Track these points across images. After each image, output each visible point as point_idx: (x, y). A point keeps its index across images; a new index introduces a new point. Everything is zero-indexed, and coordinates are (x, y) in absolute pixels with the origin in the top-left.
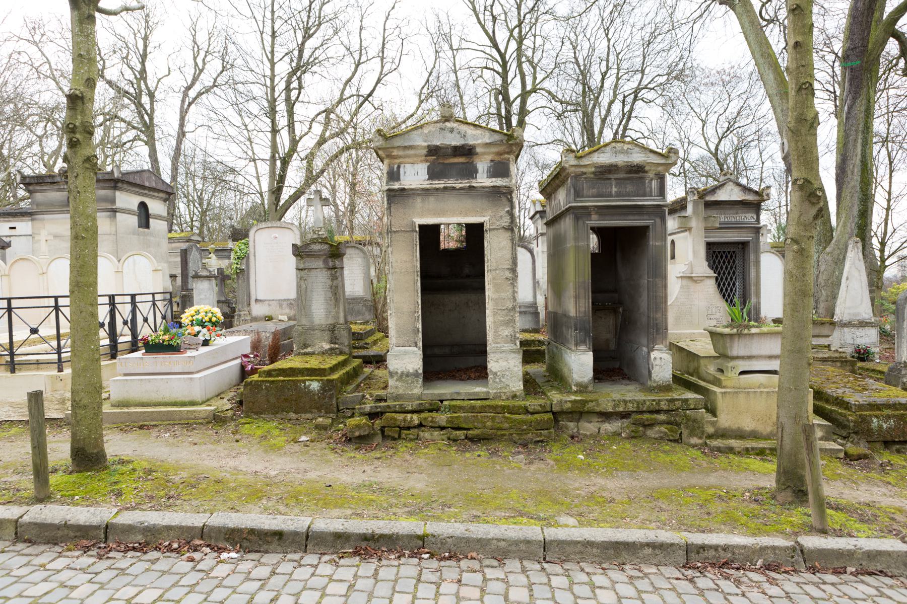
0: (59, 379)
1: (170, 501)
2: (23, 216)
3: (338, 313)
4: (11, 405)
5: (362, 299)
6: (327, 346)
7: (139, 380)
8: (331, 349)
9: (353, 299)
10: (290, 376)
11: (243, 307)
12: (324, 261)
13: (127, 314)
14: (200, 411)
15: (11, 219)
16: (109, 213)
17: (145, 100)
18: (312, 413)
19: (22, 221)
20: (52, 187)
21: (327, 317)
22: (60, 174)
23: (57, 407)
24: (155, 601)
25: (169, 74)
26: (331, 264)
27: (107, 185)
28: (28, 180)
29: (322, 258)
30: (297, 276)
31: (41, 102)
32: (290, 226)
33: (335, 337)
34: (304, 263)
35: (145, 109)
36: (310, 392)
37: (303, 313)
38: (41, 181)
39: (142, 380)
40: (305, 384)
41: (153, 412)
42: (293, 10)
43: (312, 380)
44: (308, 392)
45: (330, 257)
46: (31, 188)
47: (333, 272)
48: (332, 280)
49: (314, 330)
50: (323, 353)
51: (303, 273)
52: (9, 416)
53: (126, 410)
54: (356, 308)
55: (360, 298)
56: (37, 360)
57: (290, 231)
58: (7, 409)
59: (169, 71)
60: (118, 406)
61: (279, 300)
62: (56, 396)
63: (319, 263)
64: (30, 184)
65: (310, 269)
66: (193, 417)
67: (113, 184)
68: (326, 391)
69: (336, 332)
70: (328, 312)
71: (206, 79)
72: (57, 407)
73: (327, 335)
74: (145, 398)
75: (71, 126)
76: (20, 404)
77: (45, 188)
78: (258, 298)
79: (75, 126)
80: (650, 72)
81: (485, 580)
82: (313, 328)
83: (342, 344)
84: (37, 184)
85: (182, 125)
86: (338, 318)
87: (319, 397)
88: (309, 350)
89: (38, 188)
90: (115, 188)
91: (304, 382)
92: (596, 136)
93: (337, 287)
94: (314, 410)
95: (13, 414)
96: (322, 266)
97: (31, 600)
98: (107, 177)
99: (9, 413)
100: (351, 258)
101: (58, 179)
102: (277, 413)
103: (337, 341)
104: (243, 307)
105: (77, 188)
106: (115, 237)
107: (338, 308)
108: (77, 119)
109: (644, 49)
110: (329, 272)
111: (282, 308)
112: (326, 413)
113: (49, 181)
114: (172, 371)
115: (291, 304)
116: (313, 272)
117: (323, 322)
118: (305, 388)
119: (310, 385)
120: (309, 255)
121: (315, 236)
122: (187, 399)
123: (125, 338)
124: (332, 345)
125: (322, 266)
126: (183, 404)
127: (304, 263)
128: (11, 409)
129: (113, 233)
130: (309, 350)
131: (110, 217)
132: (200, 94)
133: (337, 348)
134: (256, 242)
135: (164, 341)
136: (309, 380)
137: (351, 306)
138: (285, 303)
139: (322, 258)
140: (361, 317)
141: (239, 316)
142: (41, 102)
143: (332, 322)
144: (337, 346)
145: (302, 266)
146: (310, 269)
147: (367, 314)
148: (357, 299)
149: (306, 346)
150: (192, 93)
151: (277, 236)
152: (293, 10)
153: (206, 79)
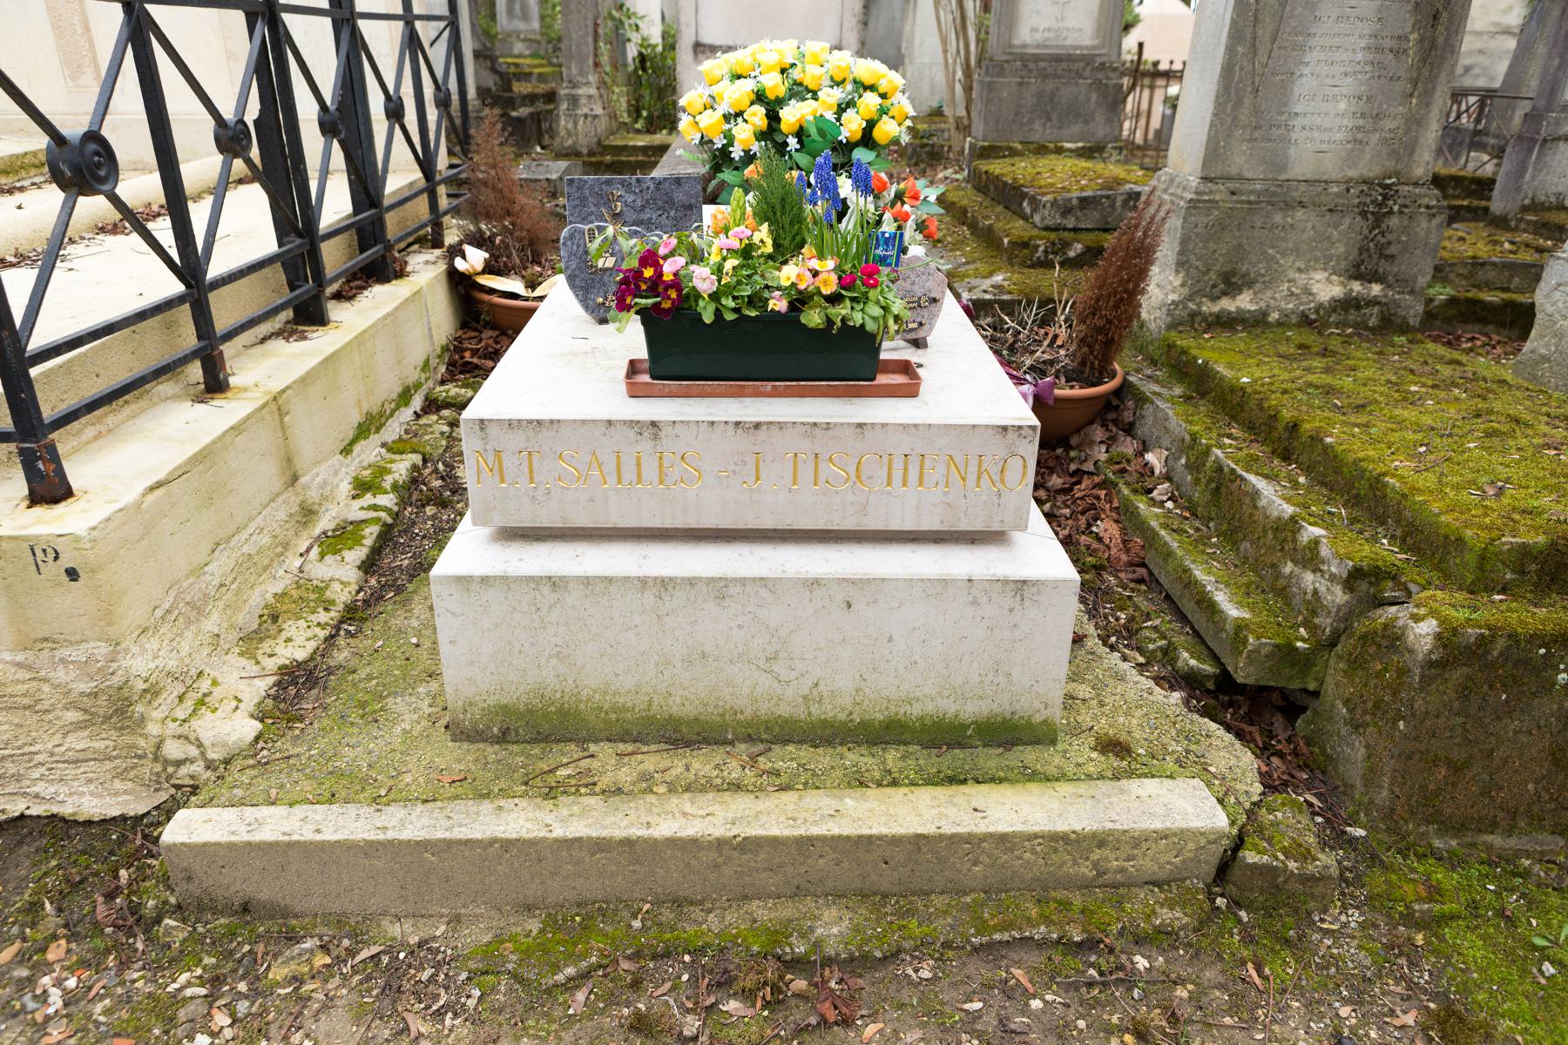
0: (54, 570)
3: (1415, 122)
5: (1088, 59)
6: (1326, 288)
8: (1348, 304)
9: (1057, 59)
11: (582, 73)
13: (326, 69)
21: (1357, 141)
31: (416, 597)
33: (1381, 248)
37: (1245, 110)
49: (1288, 206)
50: (1305, 321)
54: (1066, 93)
55: (1081, 58)
62: (60, 675)
69: (1394, 222)
70: (1370, 114)
73: (1345, 235)
78: (706, 39)
83: (1404, 283)
88: (1244, 302)
92: (255, 83)
103: (1384, 266)
104: (582, 73)
107: (1426, 103)
117: (1331, 167)
122: (972, 709)
123: (898, 465)
124: (1356, 287)
130: (1244, 302)
133: (1374, 302)
135: (800, 300)
137: (1050, 85)
140: (1075, 129)
141: (574, 101)
142: (416, 597)
143: (1374, 171)
144: (1376, 289)
148: (1069, 58)
149: (1231, 284)
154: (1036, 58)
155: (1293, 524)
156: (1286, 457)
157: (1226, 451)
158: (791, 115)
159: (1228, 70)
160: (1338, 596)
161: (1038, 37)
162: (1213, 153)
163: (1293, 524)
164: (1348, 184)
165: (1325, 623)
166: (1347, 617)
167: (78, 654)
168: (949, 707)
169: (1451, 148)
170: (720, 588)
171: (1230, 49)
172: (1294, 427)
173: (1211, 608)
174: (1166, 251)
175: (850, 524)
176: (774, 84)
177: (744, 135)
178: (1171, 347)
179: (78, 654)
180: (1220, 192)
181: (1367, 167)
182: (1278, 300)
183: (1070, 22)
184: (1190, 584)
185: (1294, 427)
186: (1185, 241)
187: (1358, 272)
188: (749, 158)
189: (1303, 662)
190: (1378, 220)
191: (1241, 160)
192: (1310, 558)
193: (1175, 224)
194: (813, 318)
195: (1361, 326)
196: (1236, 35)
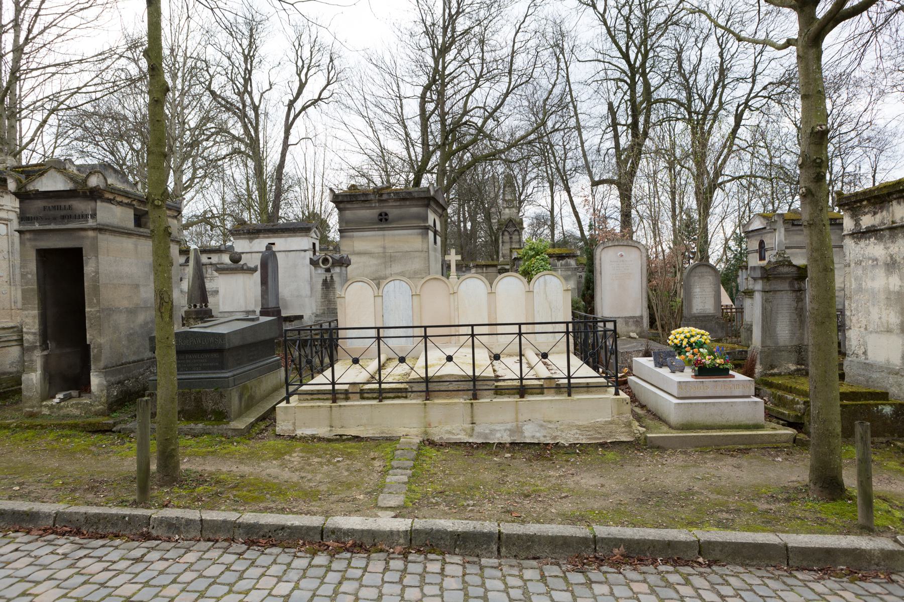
0: (625, 403)
1: (213, 502)
2: (284, 232)
4: (579, 427)
5: (713, 316)
6: (793, 367)
7: (703, 403)
8: (798, 370)
9: (705, 317)
10: (853, 400)
12: (790, 283)
14: (781, 435)
15: (270, 235)
16: (421, 231)
17: (251, 113)
18: (885, 436)
19: (281, 237)
20: (363, 205)
22: (374, 192)
23: (623, 430)
24: (55, 600)
25: (271, 88)
26: (796, 286)
27: (420, 203)
28: (340, 199)
29: (788, 281)
30: (762, 298)
32: (636, 245)
34: (770, 285)
35: (249, 119)
36: (883, 416)
38: (354, 199)
39: (706, 403)
40: (878, 408)
41: (735, 435)
42: (574, 29)
43: (884, 404)
44: (881, 416)
45: (796, 279)
46: (341, 206)
47: (799, 294)
48: (797, 302)
49: (781, 351)
50: (789, 374)
51: (768, 295)
52: (578, 439)
53: (709, 434)
56: (588, 383)
57: (635, 249)
58: (575, 431)
59: (271, 85)
60: (682, 429)
61: (625, 318)
63: (785, 286)
64: (341, 202)
65: (775, 291)
66: (774, 440)
67: (426, 202)
68: (898, 415)
69: (803, 353)
70: (793, 333)
71: (309, 94)
72: (623, 430)
73: (794, 356)
74: (709, 421)
75: (818, 161)
76: (588, 427)
77: (356, 206)
79: (822, 160)
80: (762, 81)
81: (384, 582)
82: (779, 349)
84: (348, 202)
85: (286, 137)
86: (803, 339)
87: (892, 421)
88: (776, 371)
89: (349, 206)
90: (428, 206)
91: (877, 405)
93: (802, 309)
94: (886, 434)
95: (581, 437)
96: (788, 289)
97: (124, 599)
98: (423, 195)
99: (577, 436)
100: (702, 276)
101: (372, 197)
102: (850, 437)
103: (803, 362)
105: (822, 221)
106: (427, 254)
108: (822, 153)
109: (756, 58)
110: (794, 294)
111: (628, 326)
112: (899, 437)
113: (363, 199)
114: (733, 395)
115: (637, 321)
116: (779, 295)
118: (878, 412)
119: (883, 409)
120: (776, 278)
121: (781, 259)
122: (751, 423)
124: (799, 367)
125: (788, 289)
126: (747, 427)
127: (770, 285)
128: (578, 432)
129: (425, 250)
130: (776, 371)
131: (422, 234)
132: (304, 108)
133: (803, 369)
134: (602, 259)
135: (720, 364)
136: (882, 404)
138: (631, 320)
139: (788, 281)
143: (797, 344)
144: (803, 367)
145: (767, 288)
146: (775, 291)
147: (719, 331)
148: (708, 316)
150: (298, 105)
151: (623, 254)
152: (574, 29)
153: (309, 94)
154: (699, 317)
155: (794, 399)
156: (791, 392)
157: (780, 393)
158: (692, 340)
159: (763, 327)
160: (803, 406)
161: (698, 311)
162: (763, 342)
163: (794, 399)
164: (792, 346)
165: (802, 411)
166: (805, 409)
167: (625, 416)
168: (747, 422)
169: (753, 361)
170: (714, 404)
171: (762, 323)
172: (791, 387)
173: (784, 413)
174: (758, 362)
175: (729, 395)
176: (688, 335)
177: (684, 343)
178: (762, 380)
179: (625, 416)
180: (766, 349)
181: (795, 343)
182: (783, 370)
183: (706, 307)
184: (779, 412)
185: (791, 387)
186: (761, 359)
187: (798, 363)
188: (685, 347)
189: (800, 418)
190: (800, 353)
191: (769, 343)
192: (798, 403)
193: (758, 356)
194: (721, 367)
195: (802, 375)
196: (763, 321)
